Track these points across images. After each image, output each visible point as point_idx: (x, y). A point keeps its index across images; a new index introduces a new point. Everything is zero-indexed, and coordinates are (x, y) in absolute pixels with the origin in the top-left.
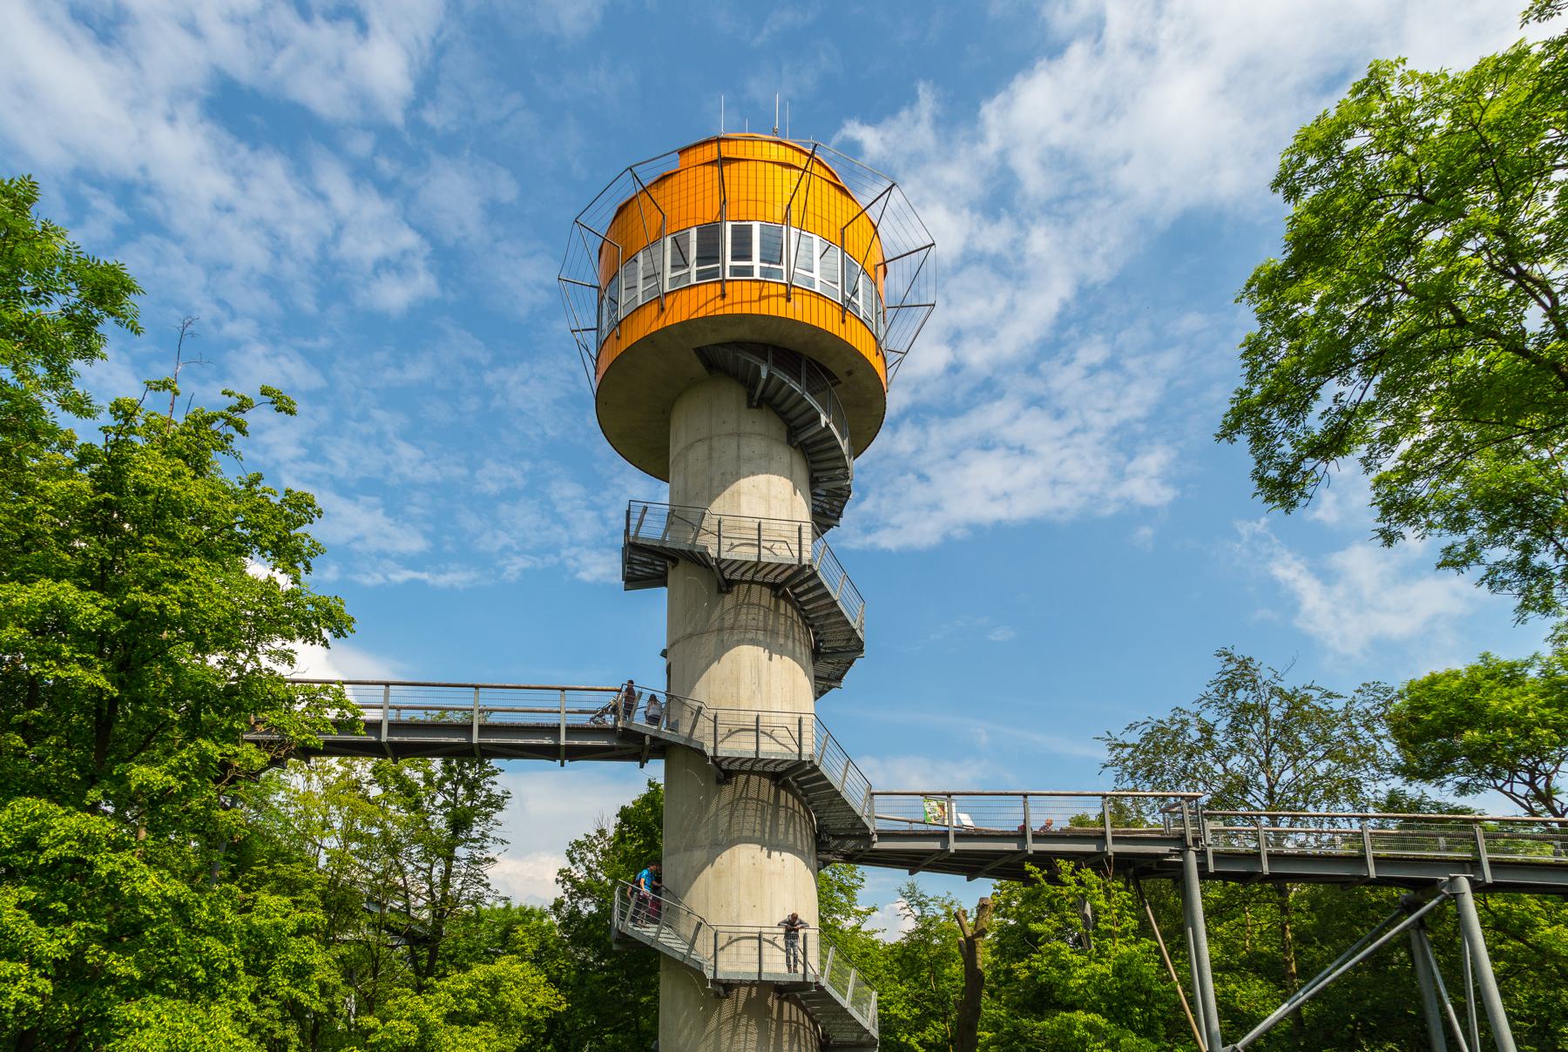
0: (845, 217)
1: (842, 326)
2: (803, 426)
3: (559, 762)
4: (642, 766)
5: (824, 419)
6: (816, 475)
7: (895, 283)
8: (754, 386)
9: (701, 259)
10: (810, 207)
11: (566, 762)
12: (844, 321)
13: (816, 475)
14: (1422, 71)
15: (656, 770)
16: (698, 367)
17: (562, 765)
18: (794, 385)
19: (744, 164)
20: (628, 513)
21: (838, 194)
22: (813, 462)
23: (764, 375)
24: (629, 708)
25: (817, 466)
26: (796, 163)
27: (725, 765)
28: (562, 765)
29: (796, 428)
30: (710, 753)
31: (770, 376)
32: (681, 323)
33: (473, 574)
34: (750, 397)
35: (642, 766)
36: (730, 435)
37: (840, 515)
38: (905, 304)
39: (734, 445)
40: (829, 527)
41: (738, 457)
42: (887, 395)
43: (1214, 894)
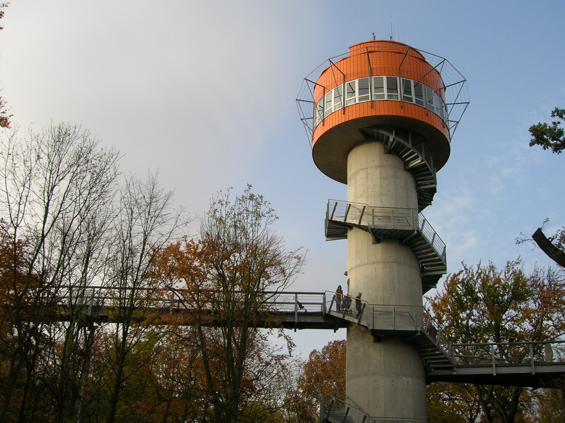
0: (328, 73)
3: (293, 329)
4: (335, 332)
6: (419, 183)
7: (105, 158)
8: (386, 143)
9: (389, 89)
11: (297, 329)
13: (419, 183)
14: (458, 272)
15: (341, 334)
16: (361, 137)
17: (295, 331)
18: (405, 144)
19: (375, 53)
20: (328, 205)
21: (421, 62)
26: (401, 51)
28: (295, 331)
31: (394, 140)
32: (353, 120)
33: (411, 166)
34: (385, 149)
35: (335, 332)
37: (432, 200)
42: (451, 144)
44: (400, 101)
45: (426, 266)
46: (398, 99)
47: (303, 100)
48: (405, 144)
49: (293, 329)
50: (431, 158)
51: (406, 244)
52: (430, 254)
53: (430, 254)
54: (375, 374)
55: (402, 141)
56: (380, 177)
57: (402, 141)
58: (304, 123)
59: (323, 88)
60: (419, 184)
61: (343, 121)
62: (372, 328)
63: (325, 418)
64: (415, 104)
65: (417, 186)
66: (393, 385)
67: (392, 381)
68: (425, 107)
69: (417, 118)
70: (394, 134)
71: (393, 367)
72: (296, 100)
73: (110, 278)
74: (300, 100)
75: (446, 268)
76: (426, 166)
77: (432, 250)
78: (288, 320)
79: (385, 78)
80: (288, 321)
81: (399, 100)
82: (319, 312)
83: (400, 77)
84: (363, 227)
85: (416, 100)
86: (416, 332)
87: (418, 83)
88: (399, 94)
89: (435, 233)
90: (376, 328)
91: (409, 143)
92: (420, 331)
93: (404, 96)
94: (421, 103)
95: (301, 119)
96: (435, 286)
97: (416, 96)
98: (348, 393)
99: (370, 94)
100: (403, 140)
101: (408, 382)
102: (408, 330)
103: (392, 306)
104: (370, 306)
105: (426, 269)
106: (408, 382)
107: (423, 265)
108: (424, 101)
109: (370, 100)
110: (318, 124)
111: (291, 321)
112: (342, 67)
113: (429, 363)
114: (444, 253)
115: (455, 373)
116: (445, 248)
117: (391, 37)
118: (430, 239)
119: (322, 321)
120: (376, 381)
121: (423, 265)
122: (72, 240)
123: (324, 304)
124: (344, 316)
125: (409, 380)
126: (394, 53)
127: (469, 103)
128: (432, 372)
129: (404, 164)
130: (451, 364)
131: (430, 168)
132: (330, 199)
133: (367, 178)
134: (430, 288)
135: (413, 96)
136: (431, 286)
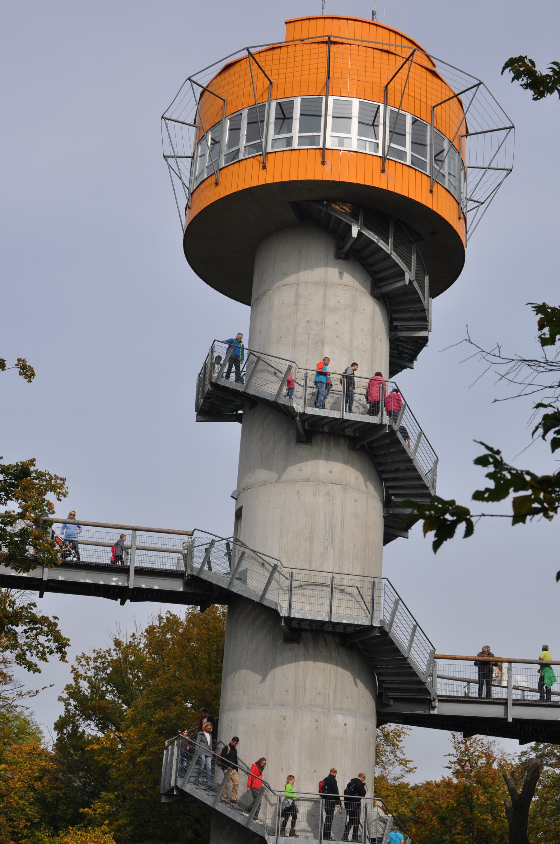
1: (429, 194)
2: (389, 278)
5: (409, 276)
6: (395, 323)
10: (411, 80)
12: (431, 191)
13: (395, 323)
22: (382, 472)
23: (355, 233)
24: (384, 821)
25: (395, 316)
27: (295, 625)
29: (381, 280)
30: (284, 613)
31: (360, 233)
36: (317, 283)
38: (492, 166)
39: (321, 293)
40: (403, 368)
41: (324, 307)
43: (326, 792)
44: (381, 157)
45: (396, 495)
46: (377, 152)
47: (175, 119)
48: (382, 244)
49: (119, 600)
50: (427, 278)
54: (283, 705)
55: (375, 238)
57: (375, 238)
58: (169, 165)
60: (396, 326)
61: (262, 183)
62: (286, 615)
64: (409, 167)
65: (392, 329)
66: (317, 728)
67: (316, 721)
68: (428, 173)
69: (417, 200)
70: (360, 223)
71: (319, 693)
72: (162, 117)
73: (119, 675)
74: (169, 119)
78: (114, 581)
79: (356, 103)
80: (114, 584)
81: (380, 154)
82: (173, 571)
83: (386, 104)
84: (283, 408)
86: (371, 628)
87: (417, 120)
88: (380, 142)
89: (422, 433)
90: (296, 614)
91: (388, 244)
92: (380, 628)
93: (389, 146)
94: (423, 164)
95: (165, 157)
96: (404, 534)
99: (321, 134)
101: (345, 725)
102: (356, 623)
103: (326, 574)
104: (285, 570)
105: (395, 500)
106: (345, 725)
107: (391, 492)
108: (428, 161)
110: (206, 177)
111: (120, 584)
112: (275, 72)
113: (385, 688)
114: (433, 471)
115: (435, 712)
116: (436, 462)
117: (374, 13)
119: (181, 590)
120: (285, 719)
121: (391, 492)
123: (187, 558)
125: (349, 720)
126: (379, 52)
127: (511, 170)
128: (391, 706)
129: (372, 283)
132: (216, 339)
134: (396, 537)
135: (408, 148)
136: (399, 533)
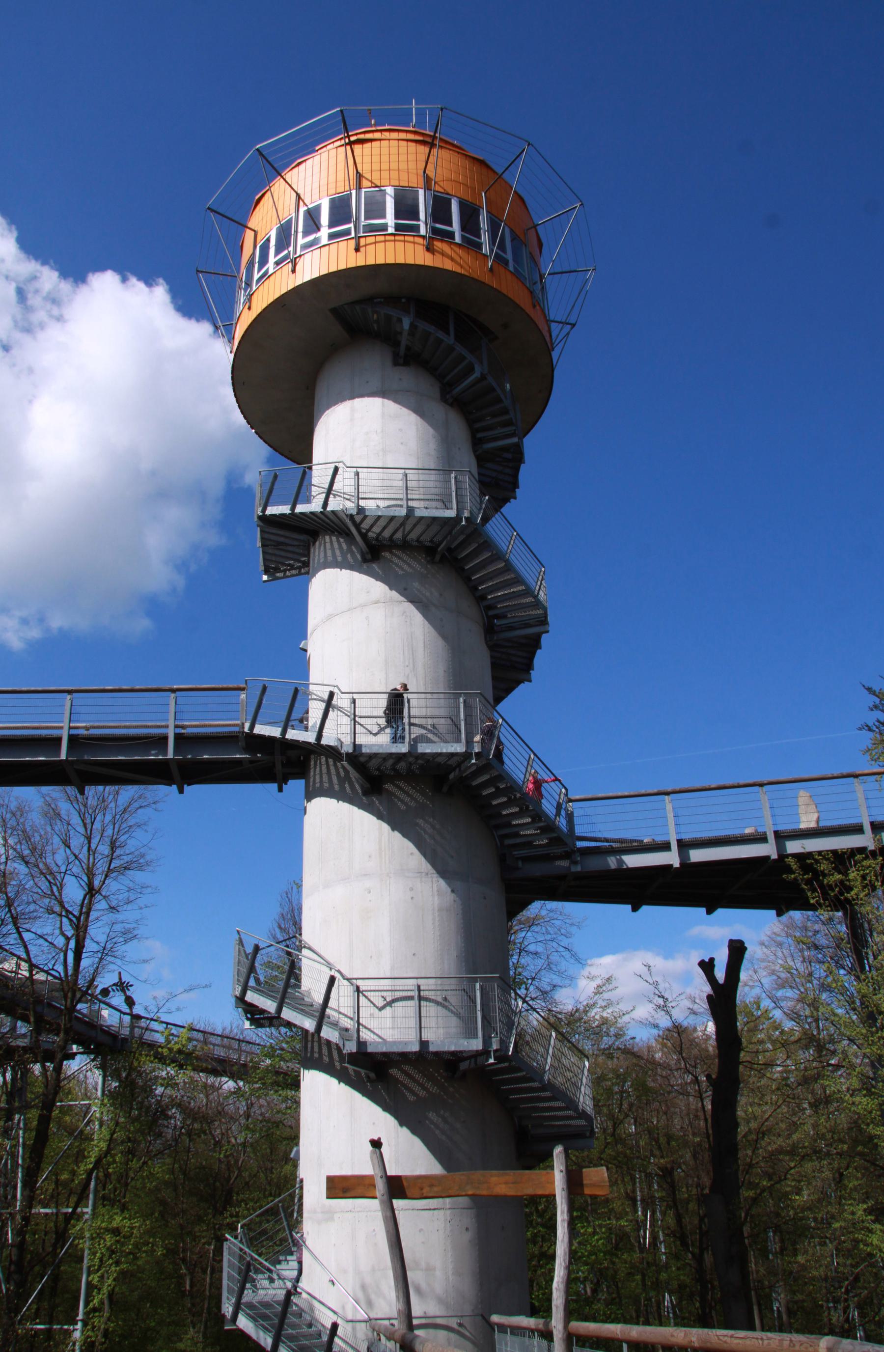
4: (280, 790)
6: (479, 435)
9: (399, 214)
13: (479, 435)
18: (440, 334)
51: (443, 560)
52: (492, 568)
53: (492, 568)
54: (365, 875)
56: (383, 415)
59: (253, 233)
63: (238, 993)
65: (476, 443)
75: (545, 615)
76: (494, 390)
77: (486, 542)
85: (463, 237)
91: (448, 333)
97: (463, 228)
98: (307, 935)
100: (433, 327)
109: (353, 235)
118: (502, 544)
120: (370, 892)
122: (623, 1181)
124: (284, 732)
130: (566, 844)
131: (502, 397)
133: (352, 420)
